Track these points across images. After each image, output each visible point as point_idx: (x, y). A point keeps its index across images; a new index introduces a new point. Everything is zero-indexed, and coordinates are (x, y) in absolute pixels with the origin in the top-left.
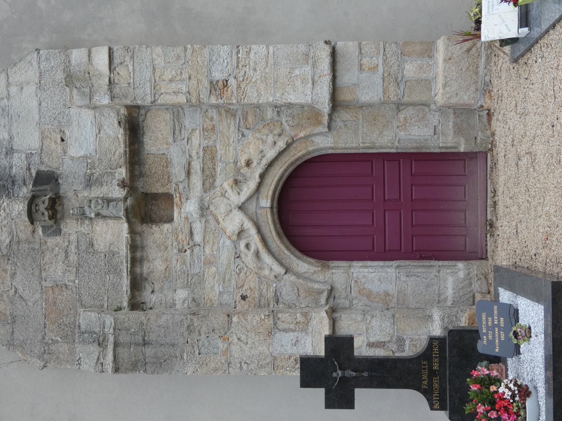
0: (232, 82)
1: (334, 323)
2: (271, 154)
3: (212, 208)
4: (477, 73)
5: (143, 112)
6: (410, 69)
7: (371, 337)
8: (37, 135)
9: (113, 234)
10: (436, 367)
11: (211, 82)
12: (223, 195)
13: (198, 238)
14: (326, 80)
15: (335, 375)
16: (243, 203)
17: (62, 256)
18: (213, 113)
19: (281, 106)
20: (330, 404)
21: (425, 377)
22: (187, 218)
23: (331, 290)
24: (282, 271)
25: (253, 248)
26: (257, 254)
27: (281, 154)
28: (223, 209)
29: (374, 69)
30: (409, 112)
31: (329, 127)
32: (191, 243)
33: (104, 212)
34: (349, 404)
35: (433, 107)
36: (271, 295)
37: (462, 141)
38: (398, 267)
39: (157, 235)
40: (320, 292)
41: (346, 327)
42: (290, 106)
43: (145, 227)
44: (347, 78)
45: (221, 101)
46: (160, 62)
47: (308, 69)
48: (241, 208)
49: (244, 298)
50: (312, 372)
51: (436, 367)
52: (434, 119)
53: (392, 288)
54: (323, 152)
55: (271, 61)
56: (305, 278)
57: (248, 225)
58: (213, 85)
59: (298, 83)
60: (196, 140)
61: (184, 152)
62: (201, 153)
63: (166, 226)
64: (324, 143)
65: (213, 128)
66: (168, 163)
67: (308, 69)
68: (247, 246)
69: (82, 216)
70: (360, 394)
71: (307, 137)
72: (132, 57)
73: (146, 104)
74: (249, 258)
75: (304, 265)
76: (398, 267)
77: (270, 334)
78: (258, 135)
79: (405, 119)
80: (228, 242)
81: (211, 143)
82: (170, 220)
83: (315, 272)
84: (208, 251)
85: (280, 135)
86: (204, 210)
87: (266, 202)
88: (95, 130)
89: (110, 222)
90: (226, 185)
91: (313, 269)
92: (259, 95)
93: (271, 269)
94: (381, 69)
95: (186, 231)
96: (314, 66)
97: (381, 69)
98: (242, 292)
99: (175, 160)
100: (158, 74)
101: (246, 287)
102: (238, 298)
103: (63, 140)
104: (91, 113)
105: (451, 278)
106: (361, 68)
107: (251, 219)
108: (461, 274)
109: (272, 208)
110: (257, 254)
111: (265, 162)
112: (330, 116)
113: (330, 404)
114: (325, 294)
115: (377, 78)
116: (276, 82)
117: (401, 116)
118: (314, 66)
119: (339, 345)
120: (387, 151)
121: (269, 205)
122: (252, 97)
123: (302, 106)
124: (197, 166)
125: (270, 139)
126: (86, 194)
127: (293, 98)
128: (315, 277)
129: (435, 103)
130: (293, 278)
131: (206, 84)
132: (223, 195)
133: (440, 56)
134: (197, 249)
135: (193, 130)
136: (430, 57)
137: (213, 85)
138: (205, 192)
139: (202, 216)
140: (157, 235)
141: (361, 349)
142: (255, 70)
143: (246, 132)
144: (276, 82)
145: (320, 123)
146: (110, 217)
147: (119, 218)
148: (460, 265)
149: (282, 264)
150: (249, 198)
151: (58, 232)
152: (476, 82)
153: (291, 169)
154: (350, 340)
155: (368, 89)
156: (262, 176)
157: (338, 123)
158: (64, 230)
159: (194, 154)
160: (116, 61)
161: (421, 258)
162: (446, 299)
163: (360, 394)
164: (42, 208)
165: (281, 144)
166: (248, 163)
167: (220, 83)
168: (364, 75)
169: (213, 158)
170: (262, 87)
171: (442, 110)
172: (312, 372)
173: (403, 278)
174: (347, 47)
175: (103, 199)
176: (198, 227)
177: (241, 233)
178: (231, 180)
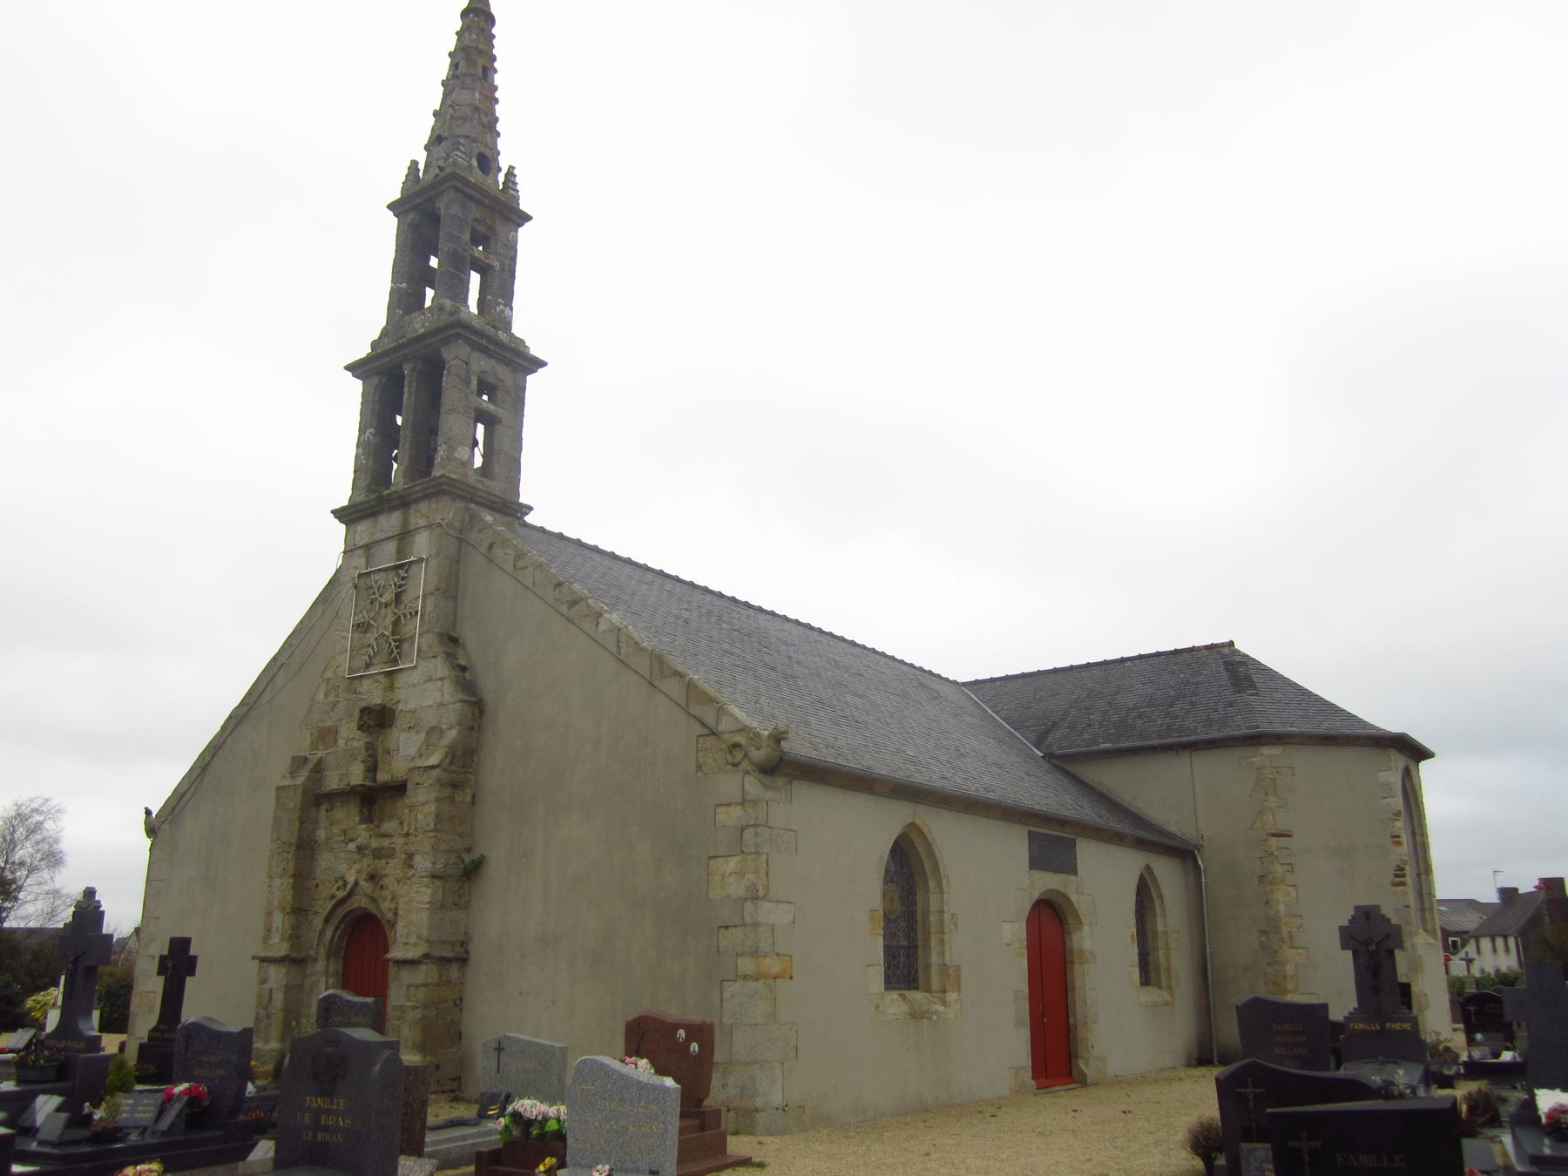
46: (426, 809)
47: (413, 940)
67: (413, 940)
106: (409, 986)
110: (333, 897)
118: (415, 944)
137: (410, 856)
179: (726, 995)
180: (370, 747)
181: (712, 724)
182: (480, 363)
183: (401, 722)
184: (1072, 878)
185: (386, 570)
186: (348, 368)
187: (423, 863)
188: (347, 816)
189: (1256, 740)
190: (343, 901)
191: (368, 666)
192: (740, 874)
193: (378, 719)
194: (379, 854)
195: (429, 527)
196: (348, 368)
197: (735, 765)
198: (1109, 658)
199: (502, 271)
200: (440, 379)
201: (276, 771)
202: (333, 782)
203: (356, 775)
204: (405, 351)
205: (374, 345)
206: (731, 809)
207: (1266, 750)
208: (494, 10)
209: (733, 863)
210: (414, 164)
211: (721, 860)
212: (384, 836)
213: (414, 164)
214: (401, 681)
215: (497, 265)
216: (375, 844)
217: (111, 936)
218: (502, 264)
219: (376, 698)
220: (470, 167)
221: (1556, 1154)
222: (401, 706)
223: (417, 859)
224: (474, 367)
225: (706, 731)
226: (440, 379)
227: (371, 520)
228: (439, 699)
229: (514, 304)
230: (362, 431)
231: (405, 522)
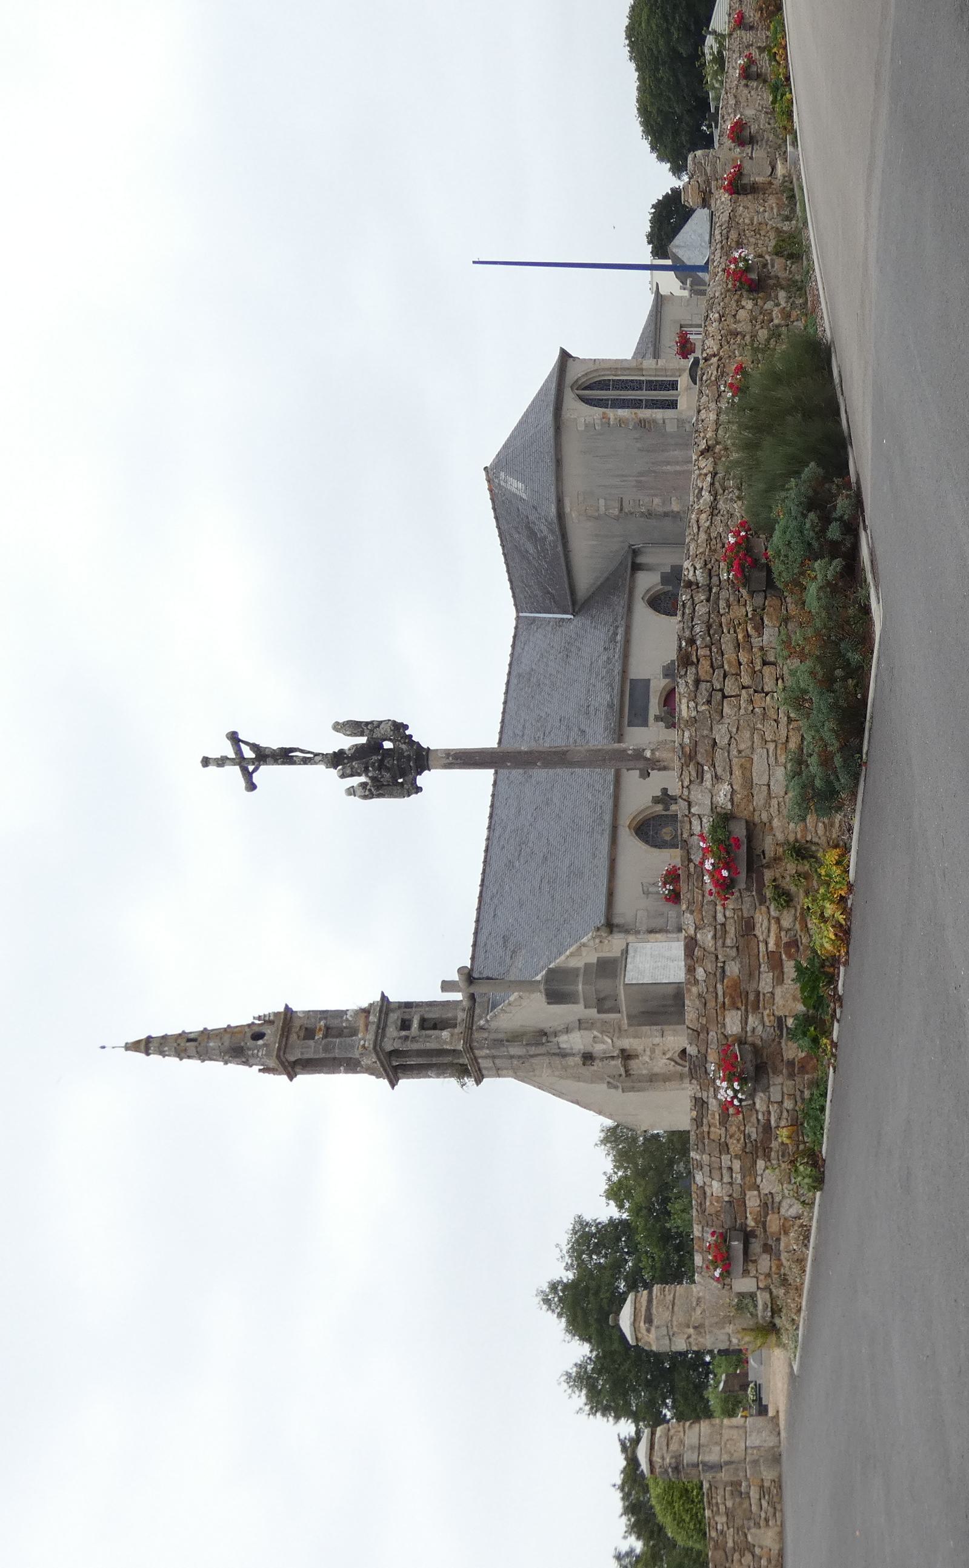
180: (602, 1059)
182: (392, 1031)
183: (590, 1049)
184: (652, 684)
186: (393, 1087)
187: (657, 1040)
188: (633, 1064)
189: (561, 515)
190: (676, 1063)
193: (588, 1058)
194: (653, 1051)
196: (393, 1087)
198: (513, 602)
199: (326, 1018)
201: (617, 1095)
202: (622, 1071)
203: (618, 1062)
207: (567, 510)
208: (143, 1036)
210: (260, 1070)
213: (260, 1070)
215: (322, 1023)
216: (648, 1053)
218: (321, 1019)
220: (265, 1045)
224: (395, 1034)
229: (344, 1009)
230: (430, 1077)
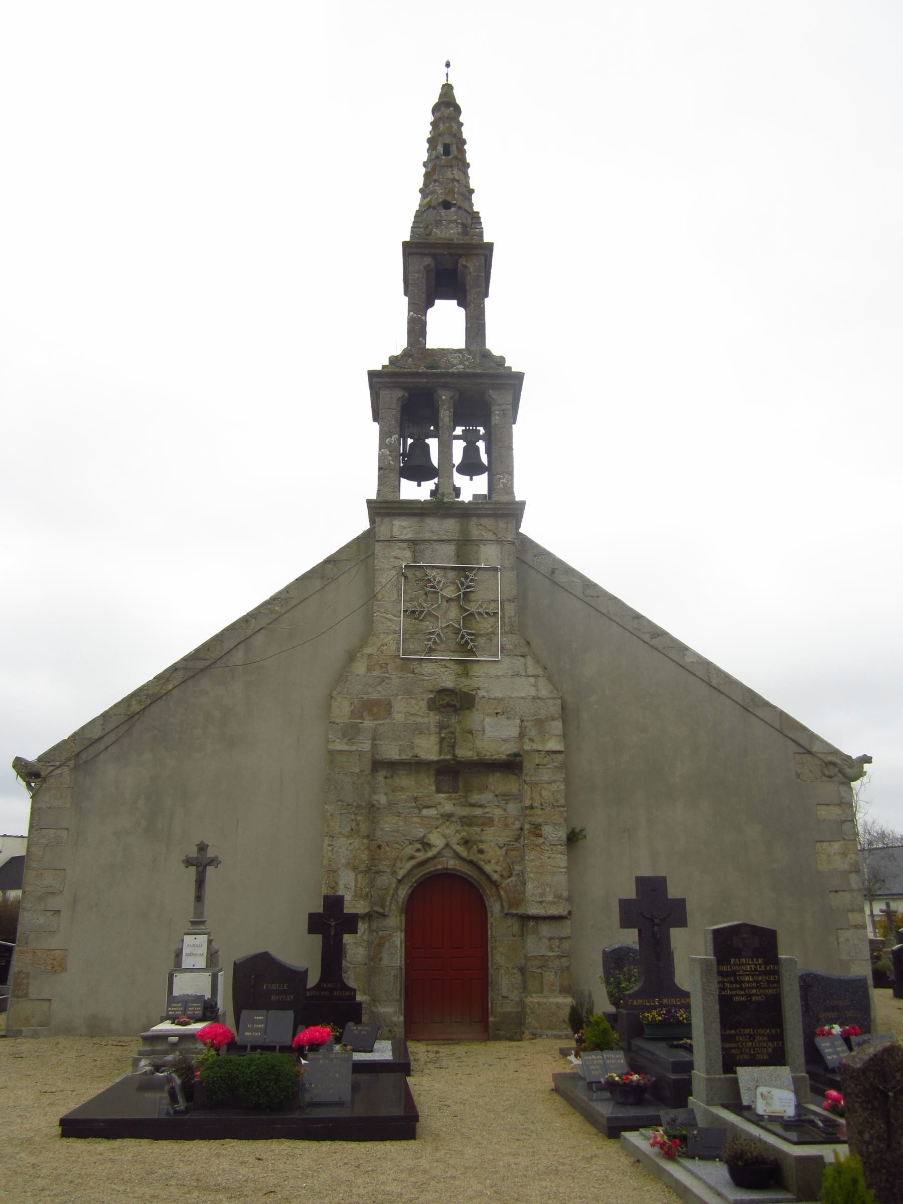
0: (541, 840)
1: (363, 917)
2: (488, 868)
3: (448, 823)
4: (548, 1028)
5: (517, 772)
6: (549, 977)
7: (354, 947)
8: (499, 695)
9: (428, 749)
10: (336, 994)
11: (540, 825)
12: (457, 831)
13: (425, 812)
14: (542, 912)
15: (332, 920)
16: (451, 848)
17: (413, 711)
18: (517, 825)
19: (524, 877)
20: (312, 916)
21: (329, 986)
22: (440, 803)
23: (383, 915)
24: (399, 877)
25: (417, 854)
26: (412, 858)
27: (488, 877)
28: (447, 832)
29: (551, 949)
30: (519, 977)
31: (506, 914)
32: (421, 807)
33: (445, 743)
34: (312, 930)
35: (523, 995)
36: (381, 867)
37: (497, 1019)
38: (401, 968)
39: (427, 785)
40: (383, 906)
41: (362, 927)
42: (524, 884)
43: (433, 772)
44: (545, 929)
45: (526, 832)
46: (554, 787)
47: (550, 898)
48: (447, 845)
49: (379, 847)
50: (333, 903)
51: (336, 994)
52: (515, 996)
53: (385, 962)
54: (489, 909)
55: (555, 870)
56: (393, 894)
57: (434, 851)
58: (538, 826)
59: (539, 891)
60: (498, 812)
61: (488, 802)
62: (488, 815)
63: (434, 788)
64: (495, 909)
65: (506, 825)
66: (481, 791)
67: (550, 898)
68: (418, 850)
69: (441, 727)
70: (318, 938)
71: (500, 897)
72: (556, 767)
73: (524, 776)
74: (409, 850)
75: (403, 893)
76: (401, 968)
77: (354, 868)
78: (501, 859)
79: (514, 974)
80: (421, 835)
81: (495, 823)
82: (438, 791)
83: (398, 902)
84: (415, 819)
85: (502, 876)
86: (448, 817)
87: (452, 864)
88: (504, 737)
89: (438, 746)
90: (464, 834)
91: (400, 901)
92: (531, 861)
93: (401, 868)
94: (551, 954)
95: (430, 803)
96: (553, 903)
97: (551, 954)
98: (384, 845)
99: (483, 796)
100: (545, 786)
101: (387, 849)
102: (379, 842)
103: (497, 713)
104: (516, 734)
105: (391, 1011)
106: (551, 939)
107: (439, 853)
108: (395, 1019)
109: (447, 869)
110: (412, 858)
111: (482, 863)
112: (516, 915)
113: (312, 916)
114: (381, 911)
115: (544, 951)
116: (541, 873)
117: (516, 971)
118: (553, 903)
119: (350, 924)
120: (490, 959)
121: (449, 867)
122: (530, 855)
123: (523, 893)
124: (478, 812)
125: (499, 868)
126: (458, 730)
127: (530, 886)
128: (394, 902)
129: (526, 997)
130: (394, 886)
131: (540, 820)
132: (457, 831)
133: (560, 1000)
134: (416, 811)
135: (505, 810)
136: (560, 992)
137: (538, 826)
138: (459, 818)
139: (442, 815)
140: (427, 781)
141: (347, 938)
142: (549, 858)
143: (504, 850)
144: (541, 873)
145: (510, 906)
146: (441, 747)
147: (440, 755)
148: (402, 1018)
149: (404, 877)
150: (455, 852)
151: (430, 708)
152: (541, 1028)
153: (475, 883)
154: (354, 931)
155: (537, 945)
156: (471, 862)
157: (510, 921)
158: (432, 713)
159: (486, 810)
160: (554, 756)
161: (406, 987)
162: (376, 1007)
163: (318, 938)
164: (448, 699)
165: (495, 877)
166: (481, 851)
167: (539, 832)
168: (547, 941)
169: (484, 824)
170: (537, 863)
171: (522, 1003)
172: (333, 903)
173: (393, 972)
174: (565, 929)
175: (455, 742)
176: (432, 812)
177: (427, 845)
178: (468, 838)
179: (841, 940)
181: (808, 747)
185: (438, 568)
191: (431, 651)
192: (844, 854)
195: (499, 542)
197: (830, 777)
200: (440, 402)
204: (449, 380)
205: (393, 360)
206: (831, 808)
209: (836, 847)
211: (825, 844)
212: (474, 805)
214: (477, 670)
217: (895, 912)
219: (448, 680)
221: (490, 1024)
222: (481, 693)
223: (546, 830)
225: (801, 750)
226: (440, 402)
227: (416, 519)
228: (533, 693)
231: (465, 531)
